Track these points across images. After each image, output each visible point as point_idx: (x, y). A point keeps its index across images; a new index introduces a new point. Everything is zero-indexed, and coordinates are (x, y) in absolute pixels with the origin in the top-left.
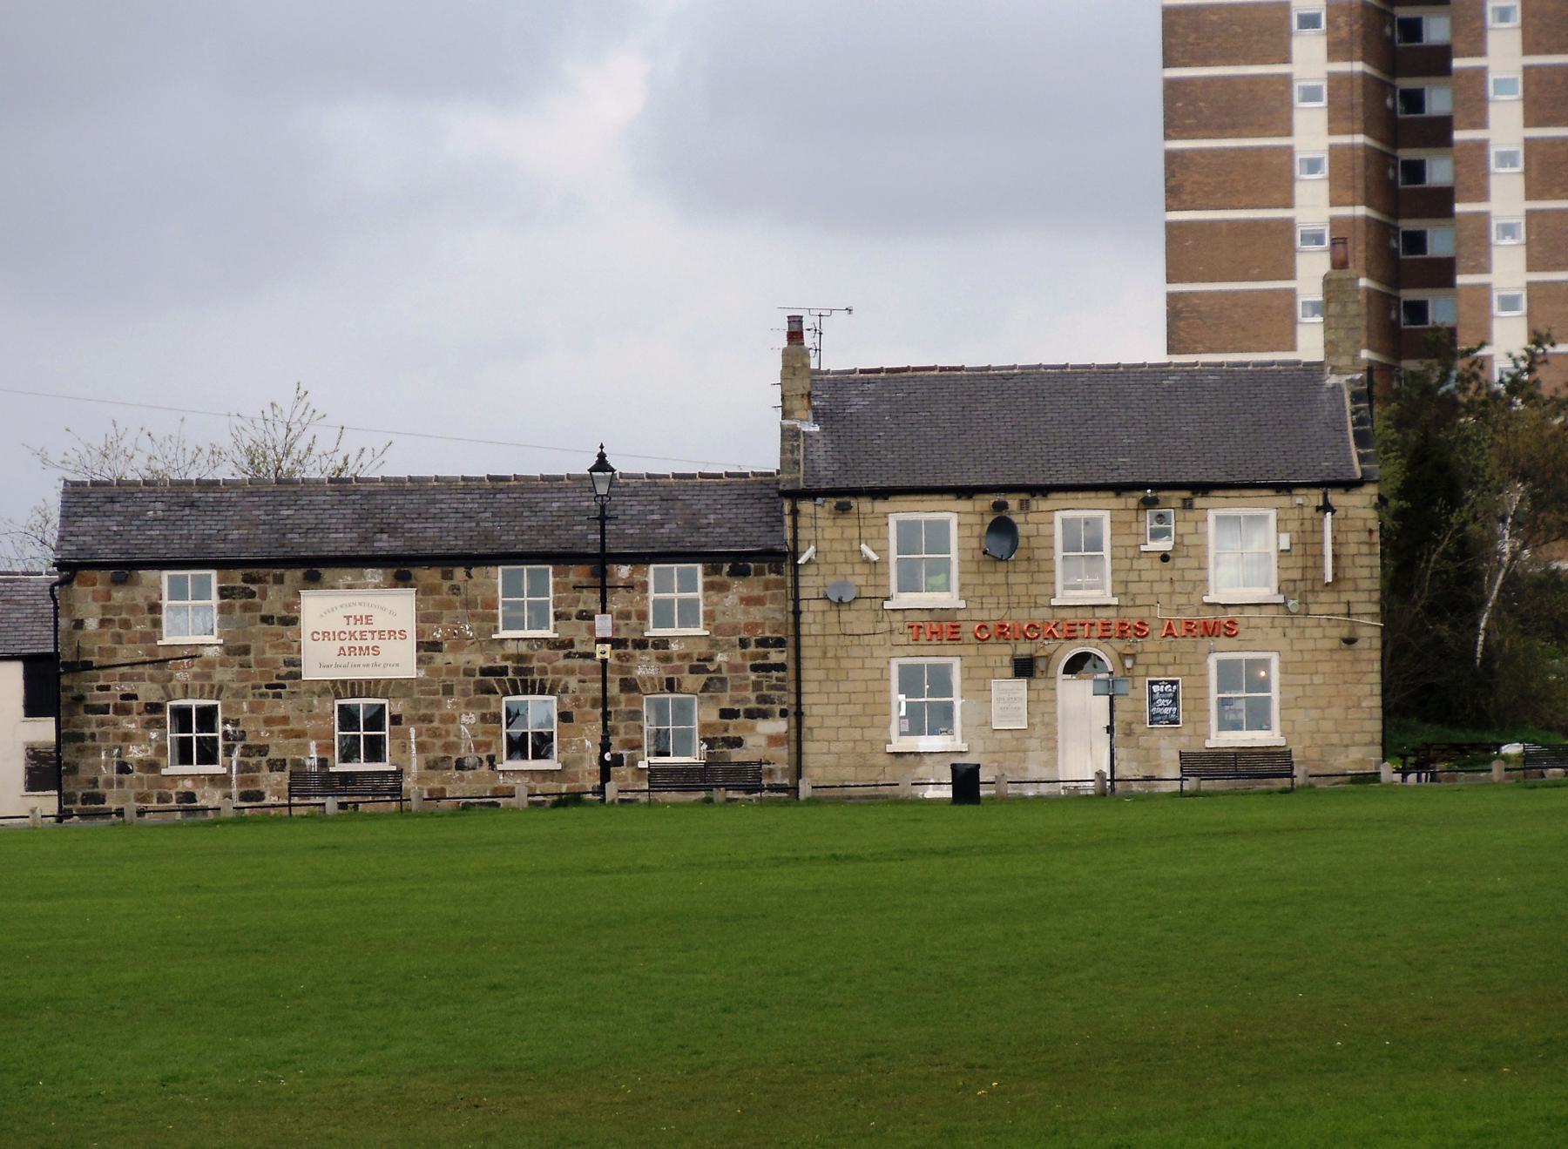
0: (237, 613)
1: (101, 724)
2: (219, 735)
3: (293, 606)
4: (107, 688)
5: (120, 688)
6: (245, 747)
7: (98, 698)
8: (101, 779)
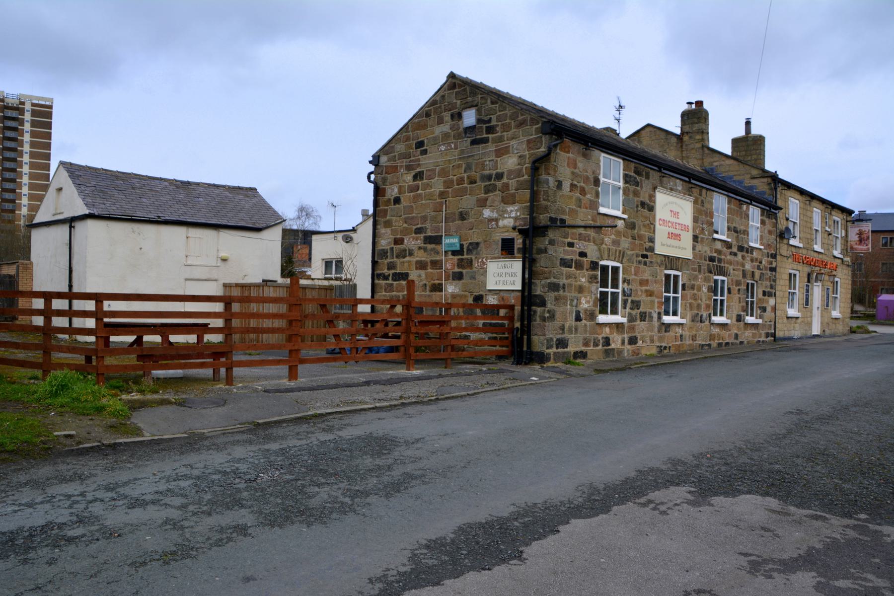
0: (631, 196)
1: (569, 276)
3: (652, 197)
6: (633, 302)
7: (565, 252)
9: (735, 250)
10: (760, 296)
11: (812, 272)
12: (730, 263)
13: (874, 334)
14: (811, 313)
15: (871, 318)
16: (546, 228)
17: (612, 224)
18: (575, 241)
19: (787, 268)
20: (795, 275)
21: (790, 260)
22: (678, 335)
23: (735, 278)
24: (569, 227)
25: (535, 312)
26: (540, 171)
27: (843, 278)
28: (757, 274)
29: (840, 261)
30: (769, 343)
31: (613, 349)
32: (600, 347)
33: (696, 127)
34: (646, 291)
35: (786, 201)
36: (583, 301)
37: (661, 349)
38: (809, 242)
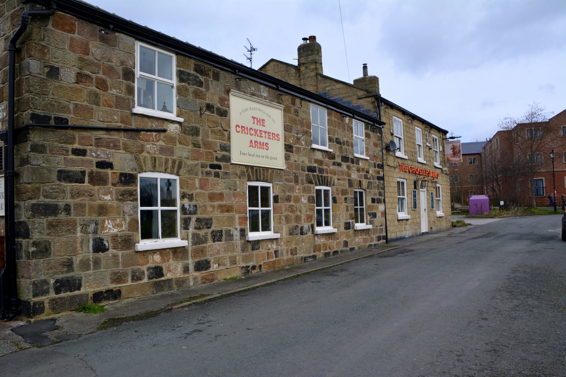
0: (191, 97)
1: (76, 194)
2: (178, 208)
3: (225, 101)
4: (83, 153)
5: (96, 154)
6: (198, 220)
7: (73, 162)
8: (77, 260)
9: (338, 160)
10: (370, 203)
11: (418, 180)
12: (335, 173)
13: (469, 227)
14: (420, 214)
15: (466, 213)
16: (27, 129)
17: (160, 128)
18: (88, 148)
19: (394, 177)
20: (403, 183)
21: (397, 170)
22: (272, 251)
23: (340, 188)
24: (75, 128)
25: (21, 245)
26: (23, 53)
27: (443, 184)
28: (365, 183)
29: (439, 171)
30: (382, 246)
31: (170, 280)
32: (146, 280)
33: (310, 58)
34: (220, 206)
35: (390, 118)
36: (109, 224)
37: (247, 270)
38: (413, 154)
